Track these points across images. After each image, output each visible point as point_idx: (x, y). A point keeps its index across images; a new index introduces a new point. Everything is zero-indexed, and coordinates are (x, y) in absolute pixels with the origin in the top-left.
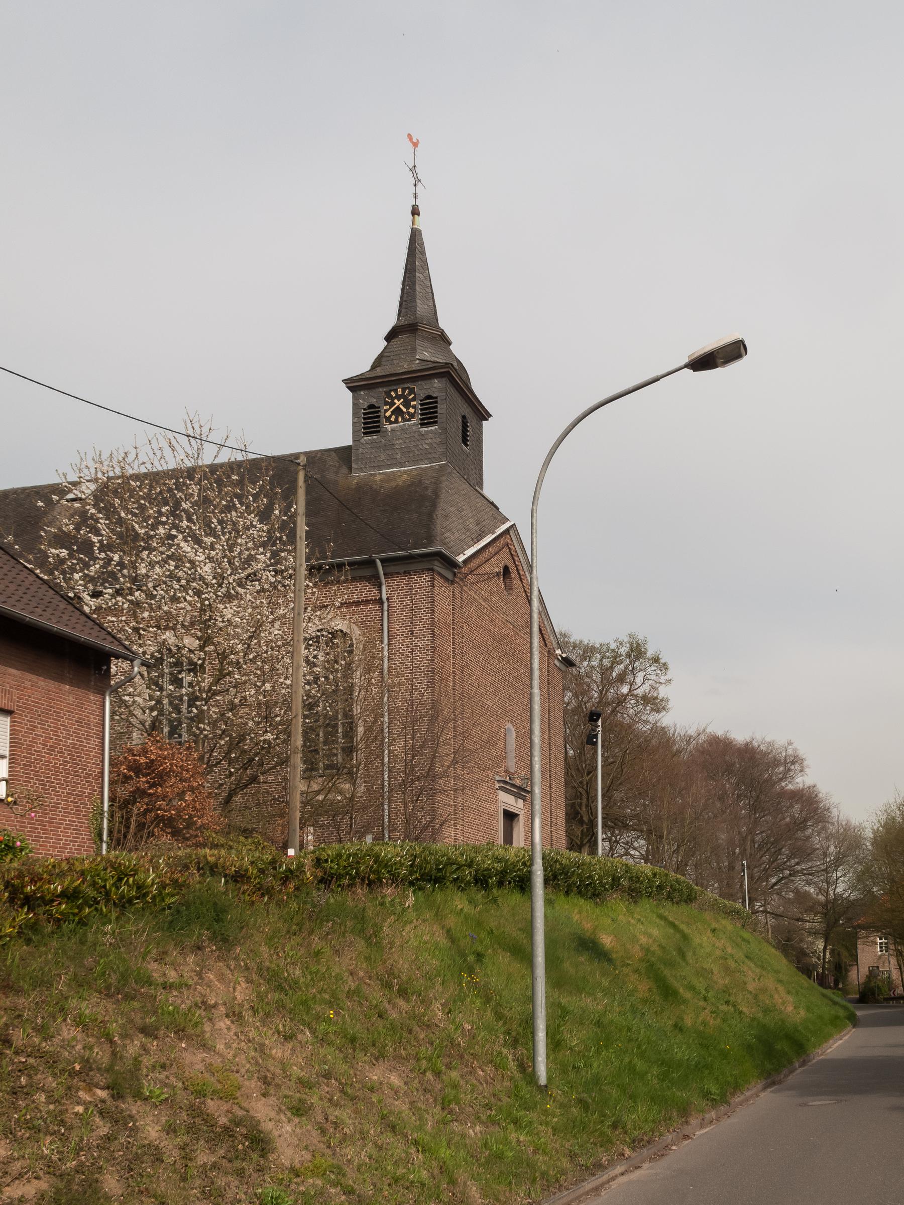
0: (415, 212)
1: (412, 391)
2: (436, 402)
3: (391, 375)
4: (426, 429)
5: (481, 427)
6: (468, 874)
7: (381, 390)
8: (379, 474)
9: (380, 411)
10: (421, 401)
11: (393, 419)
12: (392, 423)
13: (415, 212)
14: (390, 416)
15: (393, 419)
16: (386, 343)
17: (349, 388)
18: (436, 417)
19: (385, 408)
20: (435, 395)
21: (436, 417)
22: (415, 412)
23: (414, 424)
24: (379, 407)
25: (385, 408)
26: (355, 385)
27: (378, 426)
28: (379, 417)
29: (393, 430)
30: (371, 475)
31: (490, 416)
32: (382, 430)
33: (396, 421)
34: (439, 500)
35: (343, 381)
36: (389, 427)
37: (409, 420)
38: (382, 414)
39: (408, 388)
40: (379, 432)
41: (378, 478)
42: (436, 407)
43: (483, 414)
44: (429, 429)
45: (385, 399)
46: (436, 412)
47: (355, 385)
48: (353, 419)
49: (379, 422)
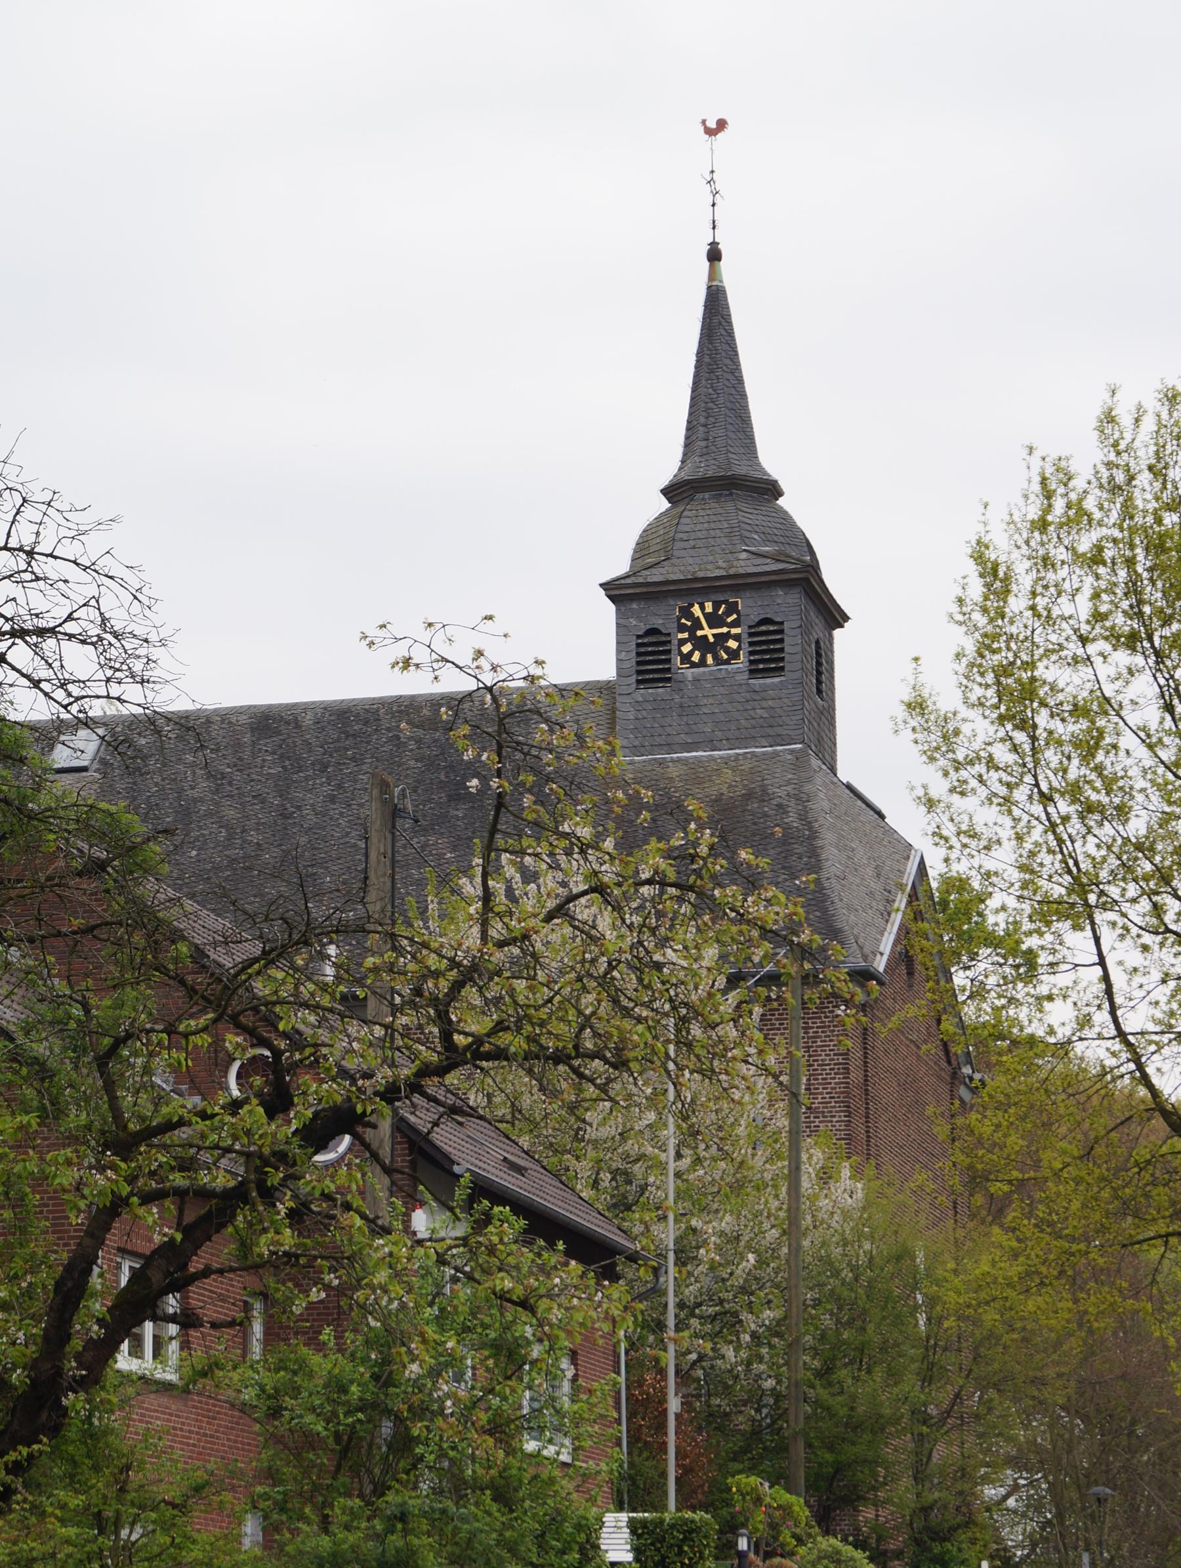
0: (714, 255)
1: (732, 609)
2: (781, 632)
3: (696, 580)
4: (762, 681)
5: (831, 637)
6: (87, 1241)
7: (672, 603)
8: (672, 760)
9: (670, 642)
10: (750, 627)
11: (696, 657)
12: (694, 665)
13: (714, 255)
14: (691, 653)
15: (696, 657)
16: (665, 505)
17: (611, 597)
18: (782, 659)
19: (680, 636)
20: (778, 619)
21: (782, 659)
22: (739, 647)
23: (738, 671)
24: (669, 634)
25: (680, 636)
26: (615, 591)
27: (668, 670)
28: (669, 652)
29: (696, 680)
30: (661, 763)
31: (846, 618)
32: (674, 677)
33: (702, 663)
34: (819, 843)
35: (601, 585)
36: (690, 673)
37: (727, 662)
38: (674, 648)
39: (726, 602)
40: (669, 680)
41: (674, 771)
42: (781, 641)
43: (835, 617)
44: (768, 681)
45: (679, 619)
46: (782, 650)
47: (615, 591)
48: (619, 652)
49: (668, 661)
